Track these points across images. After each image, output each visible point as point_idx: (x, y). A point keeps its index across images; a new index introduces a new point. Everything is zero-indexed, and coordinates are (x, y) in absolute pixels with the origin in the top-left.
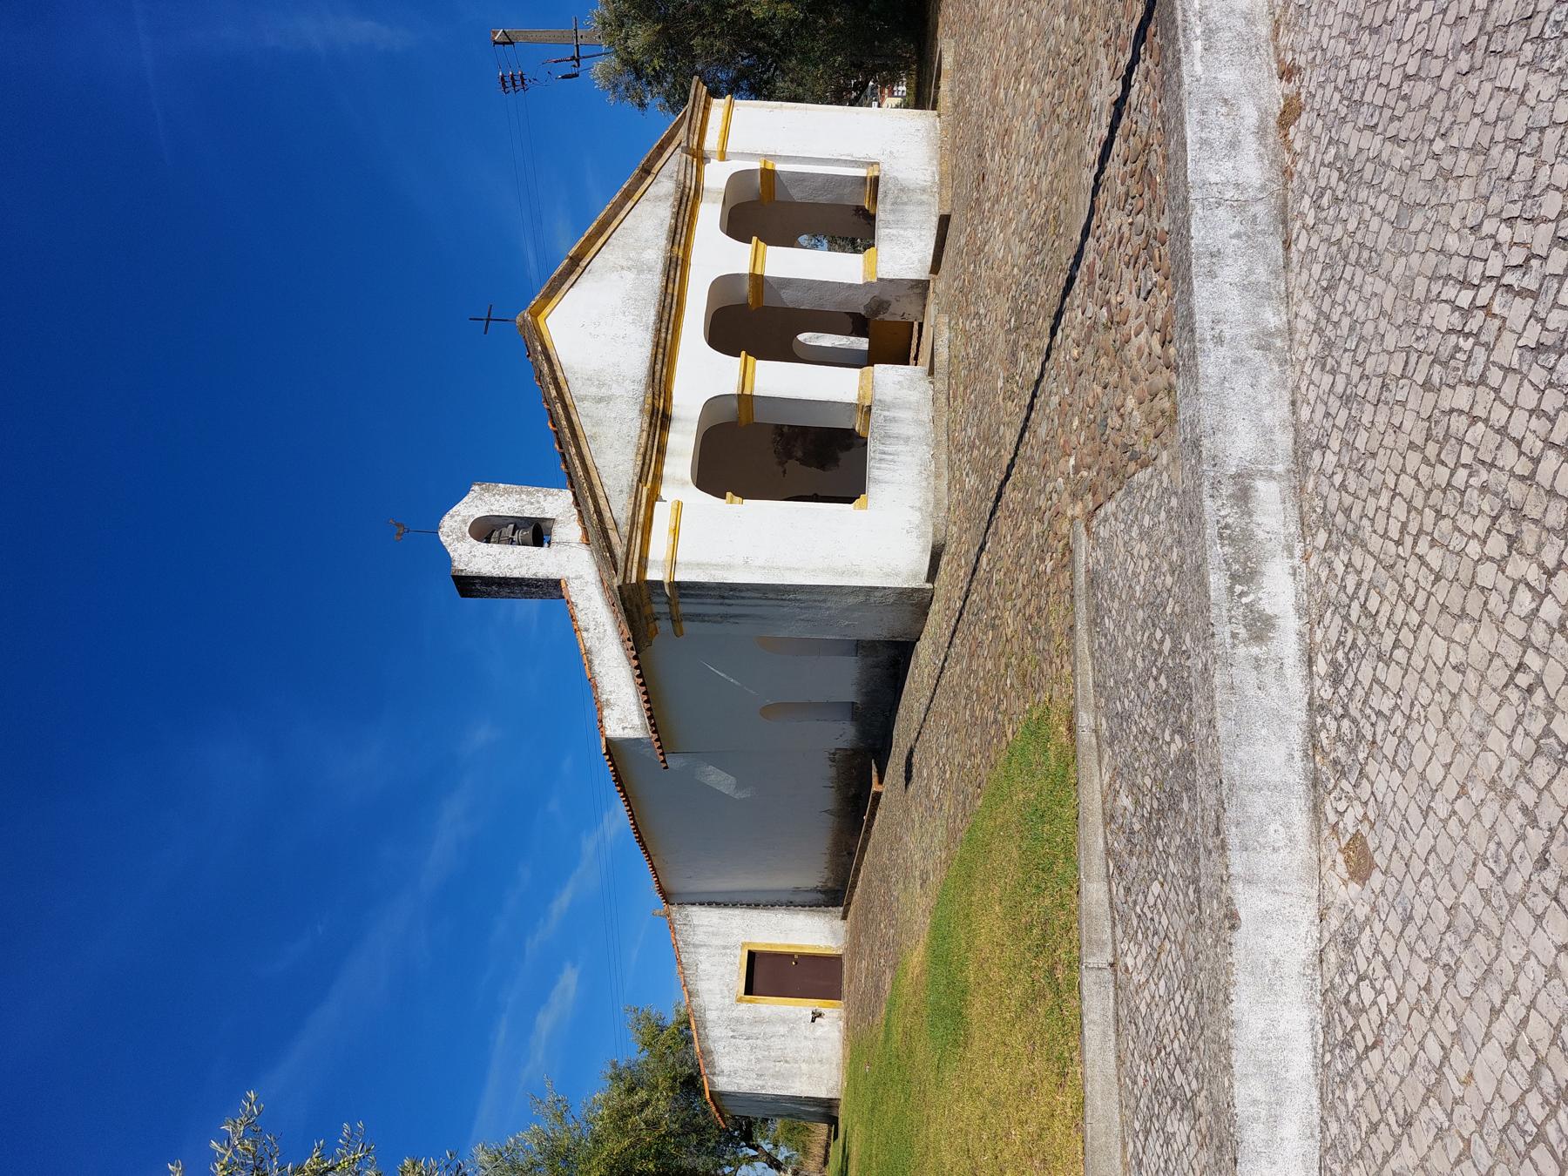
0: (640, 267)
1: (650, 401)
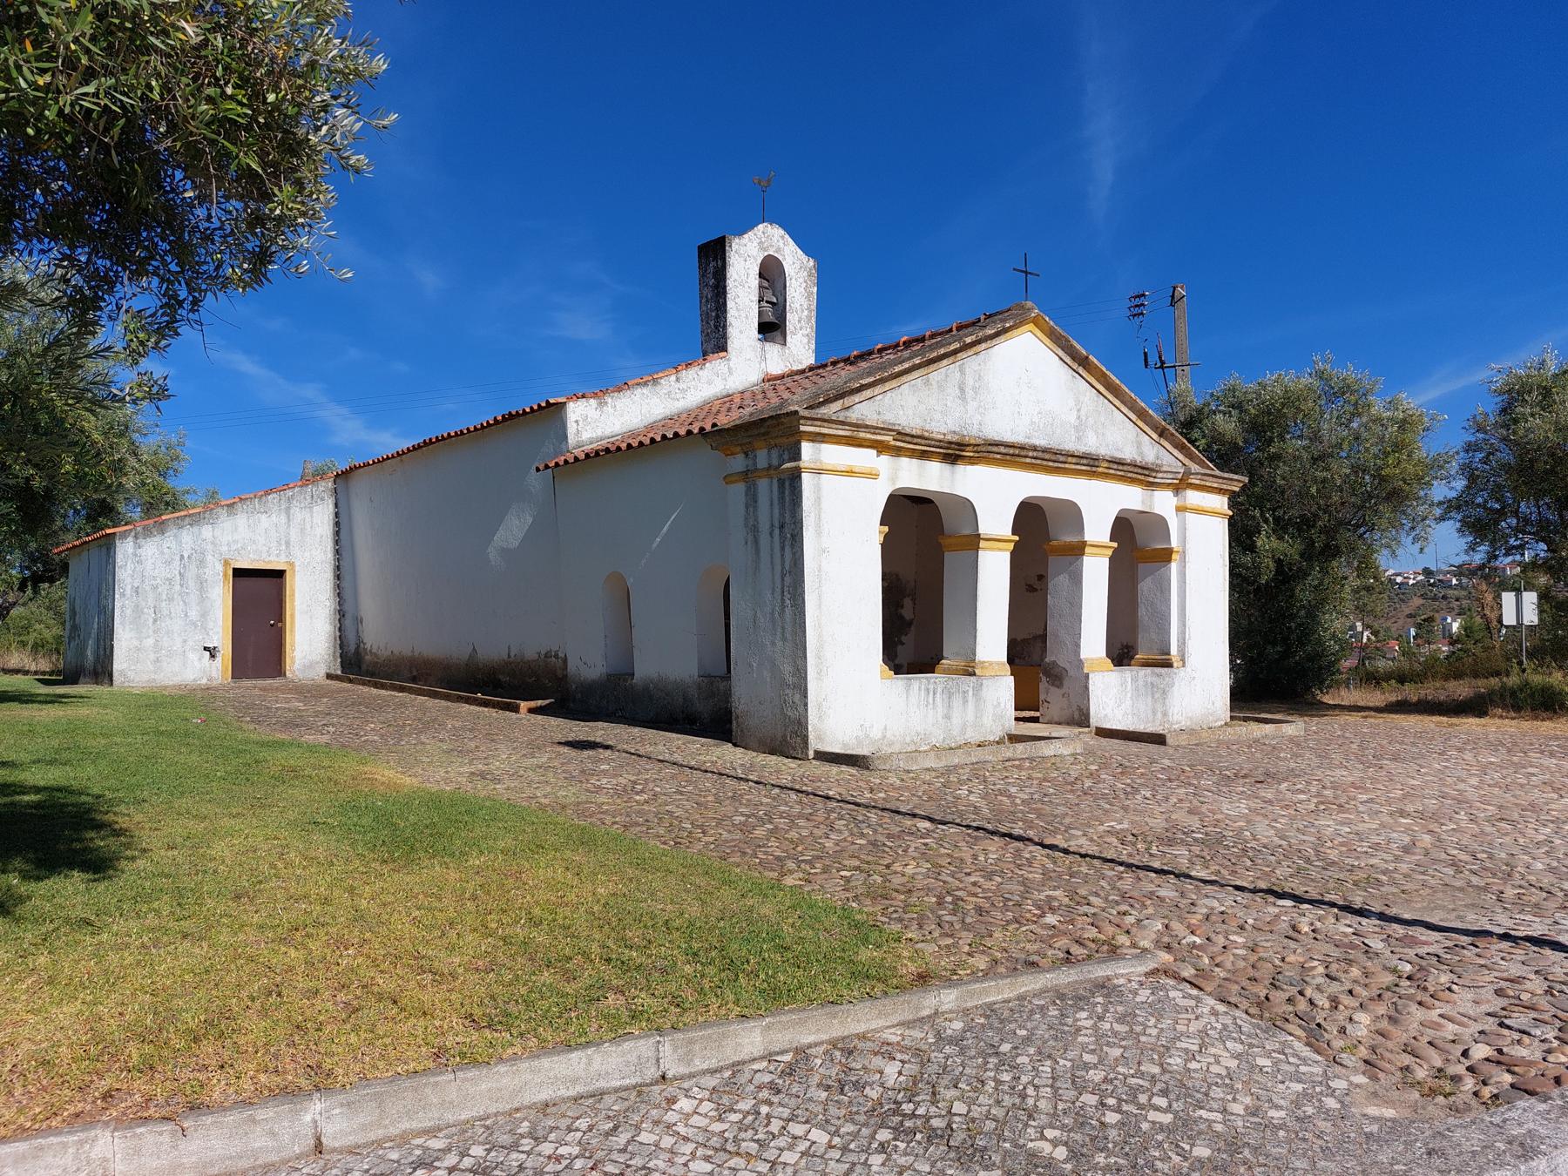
0: (1079, 428)
1: (972, 442)
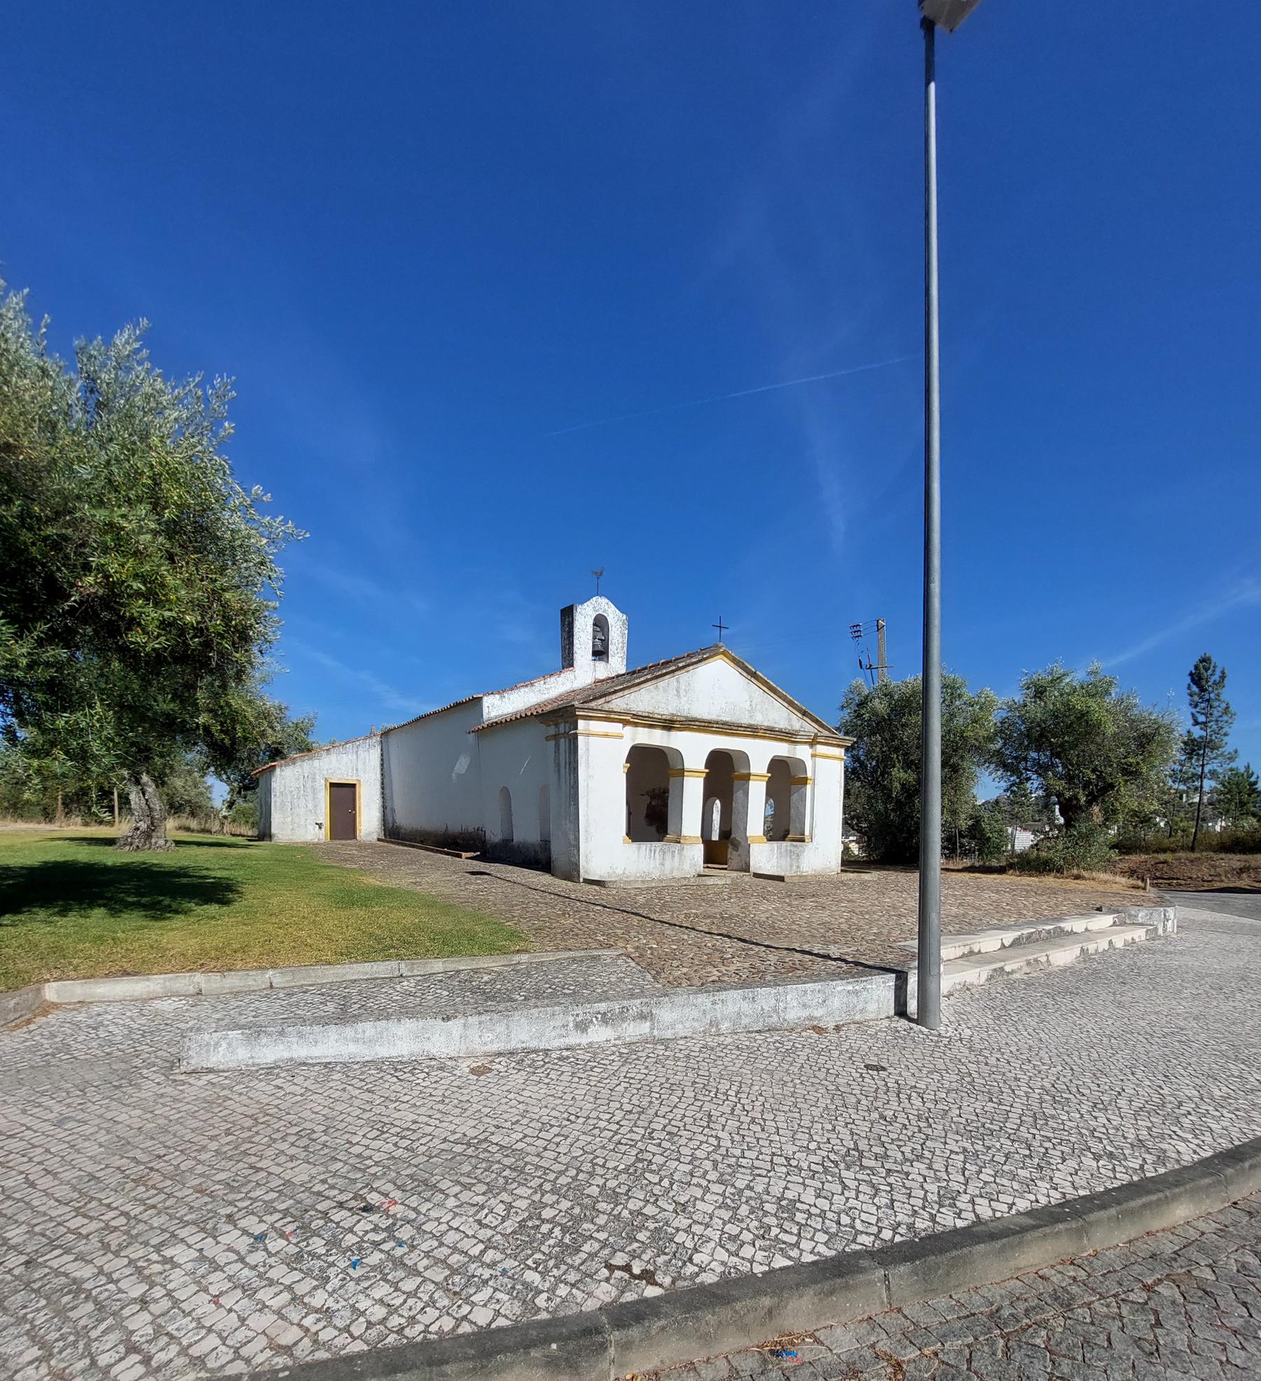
0: (751, 711)
